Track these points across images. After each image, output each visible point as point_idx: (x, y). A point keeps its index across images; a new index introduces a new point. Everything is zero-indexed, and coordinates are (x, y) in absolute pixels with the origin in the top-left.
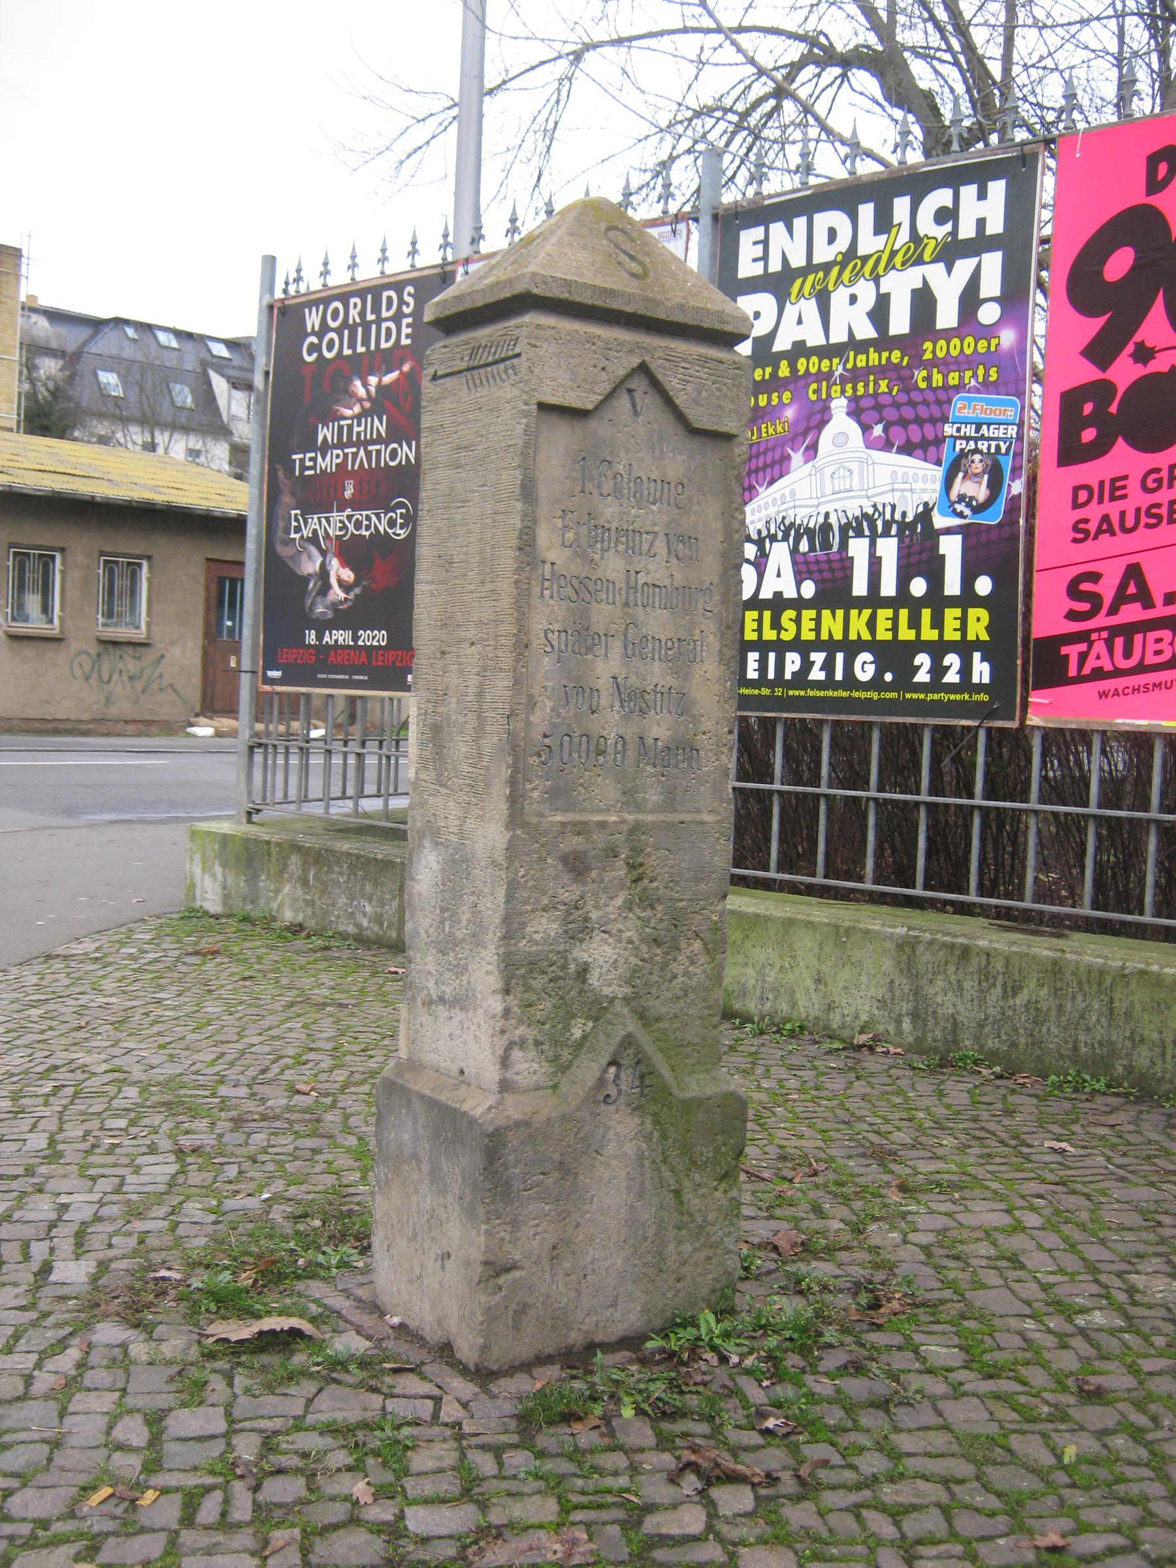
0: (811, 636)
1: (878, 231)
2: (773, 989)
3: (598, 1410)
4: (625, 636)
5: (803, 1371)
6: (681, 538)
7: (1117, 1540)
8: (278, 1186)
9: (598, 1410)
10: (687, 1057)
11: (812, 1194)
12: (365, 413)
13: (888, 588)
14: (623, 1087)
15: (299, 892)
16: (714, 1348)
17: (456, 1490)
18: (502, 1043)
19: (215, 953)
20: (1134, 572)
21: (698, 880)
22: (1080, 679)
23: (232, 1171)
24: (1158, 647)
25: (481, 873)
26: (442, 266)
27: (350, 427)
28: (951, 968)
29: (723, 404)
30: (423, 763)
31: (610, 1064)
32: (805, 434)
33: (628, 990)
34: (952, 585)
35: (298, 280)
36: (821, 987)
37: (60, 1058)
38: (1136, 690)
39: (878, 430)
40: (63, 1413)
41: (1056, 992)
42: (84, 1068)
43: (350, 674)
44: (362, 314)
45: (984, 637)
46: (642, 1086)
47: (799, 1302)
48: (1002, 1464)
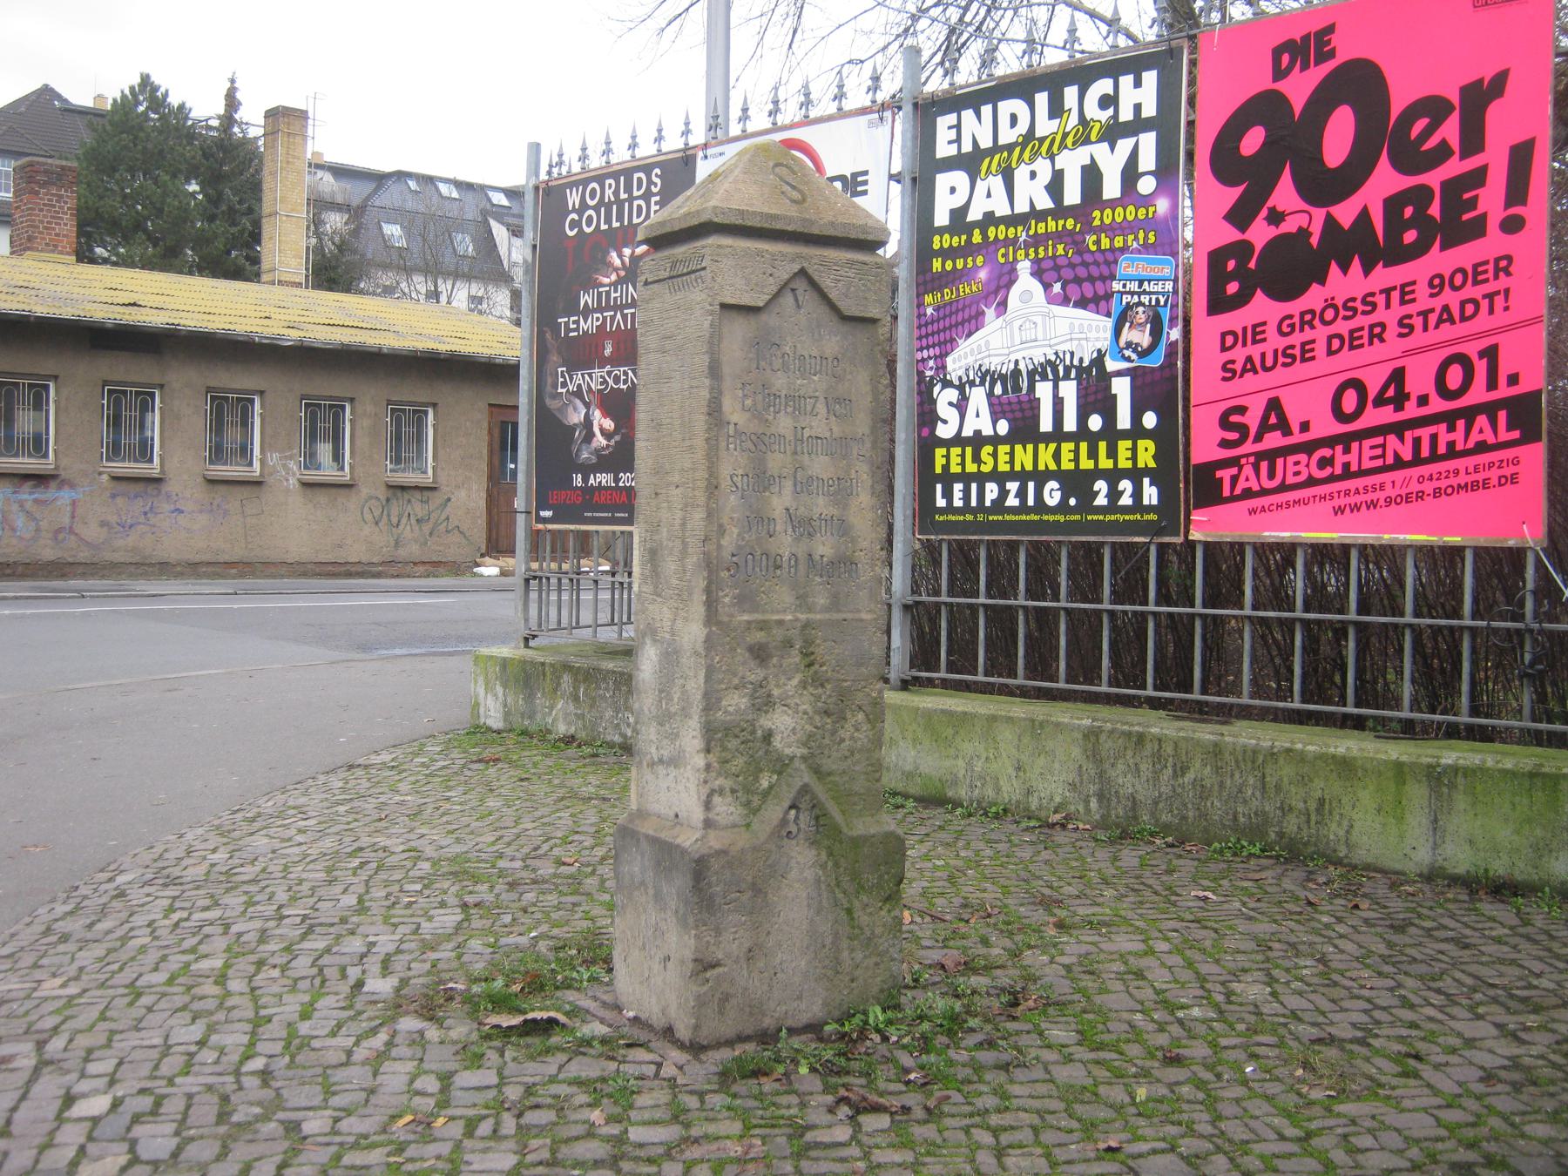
0: (1007, 468)
1: (1051, 117)
2: (980, 777)
3: (781, 1069)
5: (948, 1046)
6: (838, 401)
7: (1162, 1145)
8: (544, 928)
9: (781, 1069)
11: (984, 931)
12: (620, 281)
13: (1070, 425)
15: (571, 707)
16: (878, 1031)
17: (668, 1117)
18: (705, 791)
19: (497, 760)
20: (1274, 405)
21: (859, 665)
22: (1233, 499)
23: (507, 919)
24: (1297, 468)
25: (687, 661)
26: (684, 150)
27: (608, 293)
28: (1129, 753)
30: (644, 580)
31: (791, 808)
32: (996, 292)
33: (805, 751)
34: (1124, 421)
35: (560, 164)
37: (365, 841)
38: (1280, 506)
39: (1057, 287)
40: (375, 1075)
41: (1217, 770)
42: (385, 849)
44: (616, 193)
45: (1152, 464)
46: (817, 825)
47: (950, 1001)
48: (1088, 1103)
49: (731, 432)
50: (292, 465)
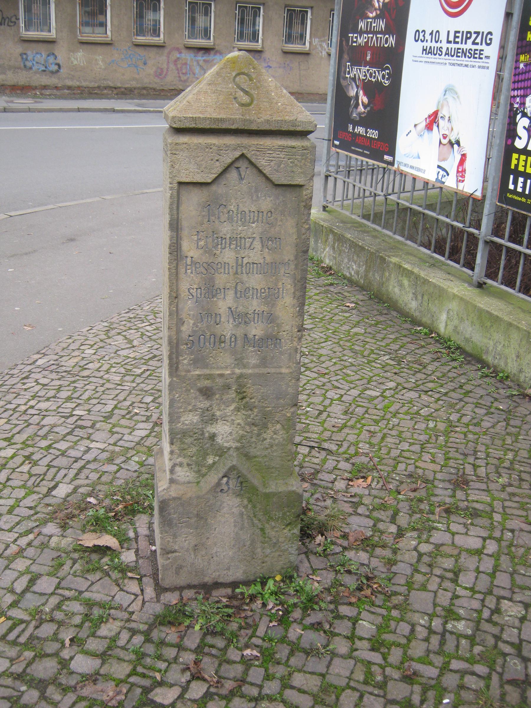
2: (499, 354)
4: (236, 288)
6: (269, 239)
10: (272, 473)
14: (231, 486)
21: (278, 398)
27: (371, 22)
29: (295, 169)
31: (223, 477)
36: (519, 360)
43: (364, 150)
49: (189, 262)
50: (325, 45)
